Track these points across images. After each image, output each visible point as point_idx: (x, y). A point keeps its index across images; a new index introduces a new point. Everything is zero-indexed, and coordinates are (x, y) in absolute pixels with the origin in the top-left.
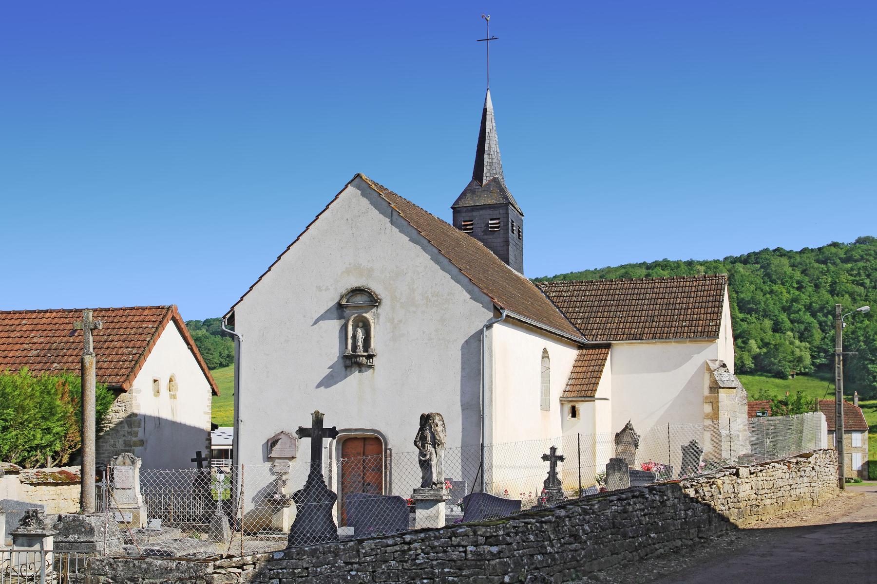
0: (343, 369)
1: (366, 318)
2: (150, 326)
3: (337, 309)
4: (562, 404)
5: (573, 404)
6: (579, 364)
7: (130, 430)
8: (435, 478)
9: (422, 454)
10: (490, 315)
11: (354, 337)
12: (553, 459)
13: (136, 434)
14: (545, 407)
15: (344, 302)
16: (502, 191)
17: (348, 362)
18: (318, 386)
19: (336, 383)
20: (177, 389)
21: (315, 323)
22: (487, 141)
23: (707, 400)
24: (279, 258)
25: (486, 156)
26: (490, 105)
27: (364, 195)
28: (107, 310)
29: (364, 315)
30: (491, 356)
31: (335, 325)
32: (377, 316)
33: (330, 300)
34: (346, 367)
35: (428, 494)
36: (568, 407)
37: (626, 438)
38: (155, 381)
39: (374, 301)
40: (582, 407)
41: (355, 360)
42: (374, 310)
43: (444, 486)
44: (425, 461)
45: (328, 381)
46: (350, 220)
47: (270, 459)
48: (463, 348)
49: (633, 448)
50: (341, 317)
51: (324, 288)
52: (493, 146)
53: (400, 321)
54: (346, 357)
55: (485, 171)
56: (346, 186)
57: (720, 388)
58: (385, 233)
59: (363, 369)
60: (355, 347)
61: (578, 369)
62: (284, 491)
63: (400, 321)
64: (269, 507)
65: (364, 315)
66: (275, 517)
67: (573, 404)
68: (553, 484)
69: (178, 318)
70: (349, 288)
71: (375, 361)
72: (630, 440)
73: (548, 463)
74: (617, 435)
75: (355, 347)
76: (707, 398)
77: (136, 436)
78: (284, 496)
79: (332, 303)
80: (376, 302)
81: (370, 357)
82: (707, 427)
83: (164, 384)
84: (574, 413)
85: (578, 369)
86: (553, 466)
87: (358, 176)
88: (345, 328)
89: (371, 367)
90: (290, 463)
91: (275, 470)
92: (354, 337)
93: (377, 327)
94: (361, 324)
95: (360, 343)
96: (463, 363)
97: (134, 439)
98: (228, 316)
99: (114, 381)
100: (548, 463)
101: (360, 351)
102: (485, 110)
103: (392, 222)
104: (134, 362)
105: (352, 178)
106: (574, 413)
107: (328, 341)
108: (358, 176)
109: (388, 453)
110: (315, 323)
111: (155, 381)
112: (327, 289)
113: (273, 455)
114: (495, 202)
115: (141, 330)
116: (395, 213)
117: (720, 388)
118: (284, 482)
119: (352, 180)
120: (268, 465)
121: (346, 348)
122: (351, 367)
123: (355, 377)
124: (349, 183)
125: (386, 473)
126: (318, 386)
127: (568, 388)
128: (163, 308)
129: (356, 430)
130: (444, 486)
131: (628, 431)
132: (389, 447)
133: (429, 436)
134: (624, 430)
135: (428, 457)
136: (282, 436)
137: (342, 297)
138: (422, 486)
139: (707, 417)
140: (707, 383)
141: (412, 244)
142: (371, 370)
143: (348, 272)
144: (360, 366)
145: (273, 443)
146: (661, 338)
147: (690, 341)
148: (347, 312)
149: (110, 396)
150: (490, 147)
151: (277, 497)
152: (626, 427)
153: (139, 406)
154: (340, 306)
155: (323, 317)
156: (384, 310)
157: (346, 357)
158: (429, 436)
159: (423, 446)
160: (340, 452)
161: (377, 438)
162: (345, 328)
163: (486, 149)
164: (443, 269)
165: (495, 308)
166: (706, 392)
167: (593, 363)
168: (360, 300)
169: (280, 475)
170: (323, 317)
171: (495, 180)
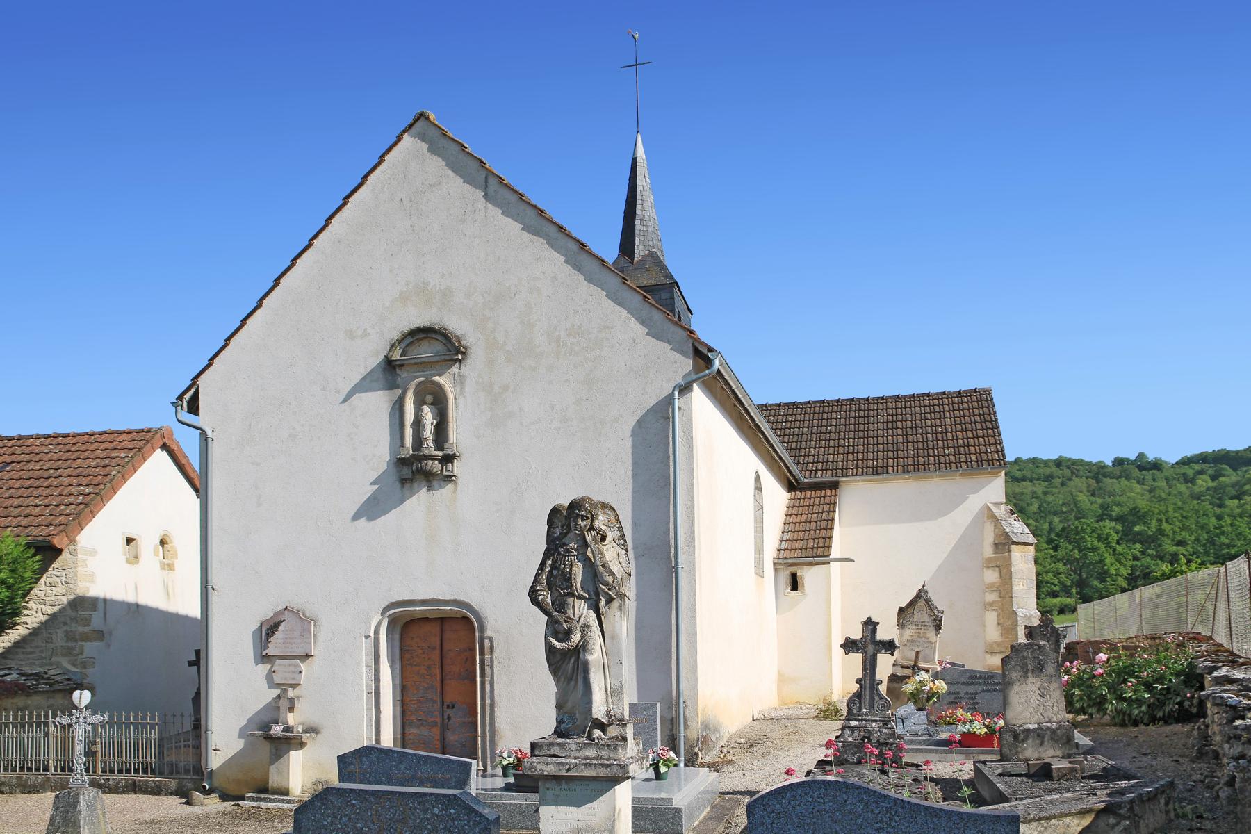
0: (398, 485)
1: (440, 387)
2: (123, 455)
3: (384, 370)
4: (776, 570)
5: (793, 569)
6: (795, 510)
7: (74, 614)
8: (599, 709)
9: (558, 629)
10: (688, 364)
11: (418, 423)
12: (871, 649)
13: (87, 622)
14: (759, 572)
15: (396, 356)
16: (663, 268)
17: (406, 472)
18: (356, 517)
19: (385, 512)
20: (175, 556)
21: (344, 401)
22: (639, 202)
23: (989, 563)
24: (277, 282)
25: (637, 222)
26: (641, 153)
27: (433, 150)
28: (65, 436)
29: (436, 378)
30: (690, 448)
31: (378, 402)
32: (460, 381)
33: (371, 354)
34: (403, 481)
35: (577, 756)
36: (785, 576)
37: (921, 615)
38: (129, 541)
39: (451, 350)
40: (809, 576)
41: (419, 466)
42: (455, 369)
43: (629, 732)
44: (566, 654)
45: (372, 509)
46: (406, 201)
47: (265, 659)
48: (634, 433)
49: (931, 633)
50: (391, 386)
51: (360, 332)
52: (647, 208)
53: (505, 388)
54: (401, 462)
55: (637, 242)
56: (399, 139)
57: (1014, 543)
58: (474, 221)
59: (435, 483)
60: (418, 441)
61: (793, 519)
62: (291, 719)
63: (505, 388)
64: (266, 748)
65: (436, 378)
66: (273, 769)
67: (793, 569)
68: (871, 707)
69: (174, 447)
70: (406, 330)
71: (457, 467)
72: (926, 619)
73: (857, 658)
74: (901, 610)
75: (418, 441)
76: (989, 560)
77: (88, 624)
78: (288, 729)
79: (376, 360)
80: (459, 352)
81: (448, 459)
82: (991, 604)
83: (148, 545)
84: (795, 584)
85: (793, 519)
86: (870, 666)
87: (422, 116)
88: (399, 406)
89: (450, 479)
90: (303, 666)
91: (277, 679)
92: (418, 423)
93: (461, 400)
94: (429, 398)
95: (429, 433)
96: (635, 463)
97: (81, 629)
98: (188, 396)
99: (39, 534)
100: (857, 658)
101: (429, 447)
102: (635, 161)
103: (486, 197)
104: (82, 506)
105: (410, 121)
106: (795, 584)
107: (367, 435)
108: (422, 116)
109: (487, 647)
110: (344, 401)
111: (129, 541)
112: (365, 334)
113: (271, 651)
114: (654, 283)
115: (107, 462)
116: (492, 181)
117: (1014, 543)
118: (292, 701)
119: (411, 126)
120: (263, 669)
121: (403, 445)
122: (411, 480)
123: (420, 501)
124: (404, 131)
125: (483, 684)
126: (356, 517)
127: (784, 545)
128: (149, 431)
129: (424, 602)
130: (629, 732)
131: (921, 603)
132: (488, 633)
133: (578, 571)
134: (912, 604)
135: (576, 637)
136: (287, 616)
137: (392, 346)
138: (559, 733)
139: (990, 588)
140: (989, 537)
141: (526, 235)
142: (450, 487)
143: (403, 298)
144: (429, 478)
145: (270, 629)
146: (916, 470)
147: (962, 475)
148: (403, 374)
149: (34, 563)
150: (643, 209)
151: (277, 730)
152: (918, 596)
153: (92, 578)
154: (390, 366)
155: (359, 388)
156: (472, 368)
157: (401, 462)
158: (578, 571)
159: (560, 606)
160: (397, 644)
161: (467, 619)
162: (399, 406)
163: (638, 212)
164: (590, 280)
165: (697, 352)
166: (988, 551)
167: (816, 509)
168: (426, 351)
169: (283, 687)
170: (359, 388)
171: (652, 255)
